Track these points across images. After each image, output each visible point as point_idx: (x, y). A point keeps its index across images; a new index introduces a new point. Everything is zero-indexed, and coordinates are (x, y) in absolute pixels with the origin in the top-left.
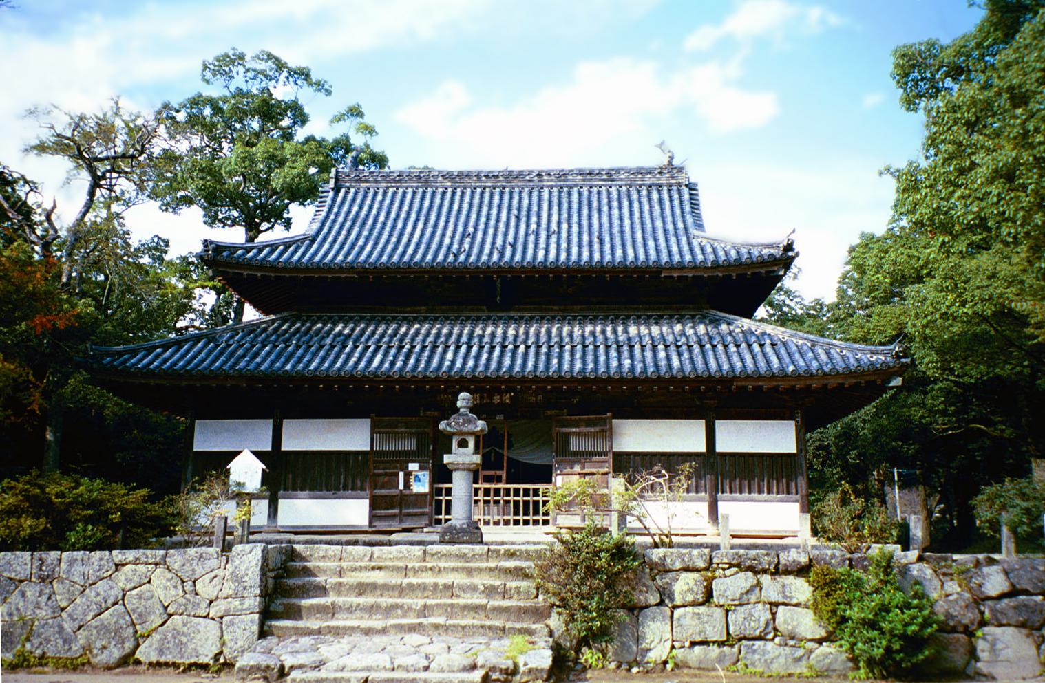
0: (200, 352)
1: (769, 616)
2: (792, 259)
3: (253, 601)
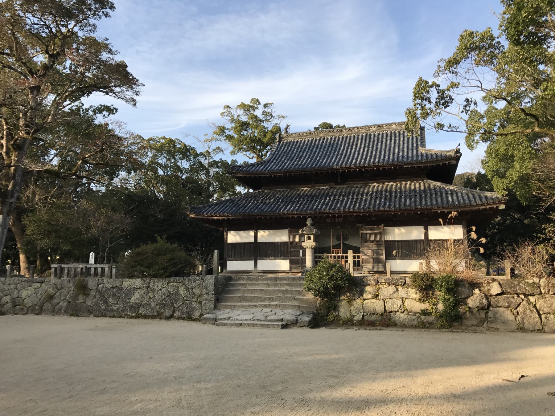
1: (402, 303)
2: (459, 157)
3: (212, 296)
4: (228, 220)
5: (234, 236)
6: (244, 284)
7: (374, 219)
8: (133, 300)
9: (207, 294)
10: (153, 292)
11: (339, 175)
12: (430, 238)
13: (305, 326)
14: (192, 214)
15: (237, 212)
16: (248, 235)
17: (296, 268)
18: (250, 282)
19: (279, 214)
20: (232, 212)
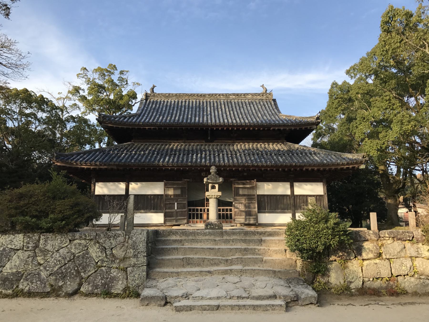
0: (98, 156)
1: (411, 264)
3: (143, 260)
4: (101, 169)
5: (102, 188)
6: (181, 241)
7: (245, 174)
8: (8, 269)
9: (135, 256)
10: (45, 255)
11: (209, 132)
12: (295, 194)
13: (312, 303)
14: (58, 162)
15: (111, 161)
16: (118, 187)
17: (170, 221)
18: (186, 238)
19: (158, 166)
20: (106, 161)
